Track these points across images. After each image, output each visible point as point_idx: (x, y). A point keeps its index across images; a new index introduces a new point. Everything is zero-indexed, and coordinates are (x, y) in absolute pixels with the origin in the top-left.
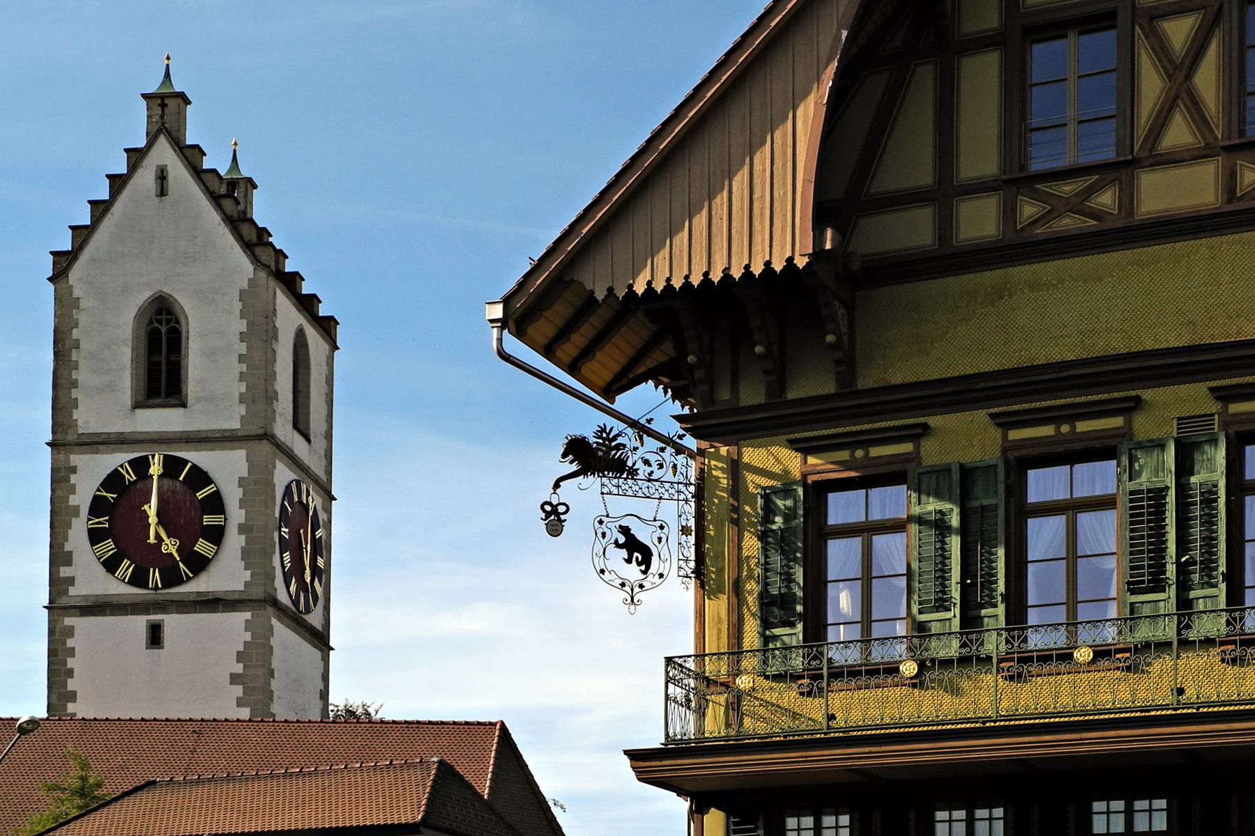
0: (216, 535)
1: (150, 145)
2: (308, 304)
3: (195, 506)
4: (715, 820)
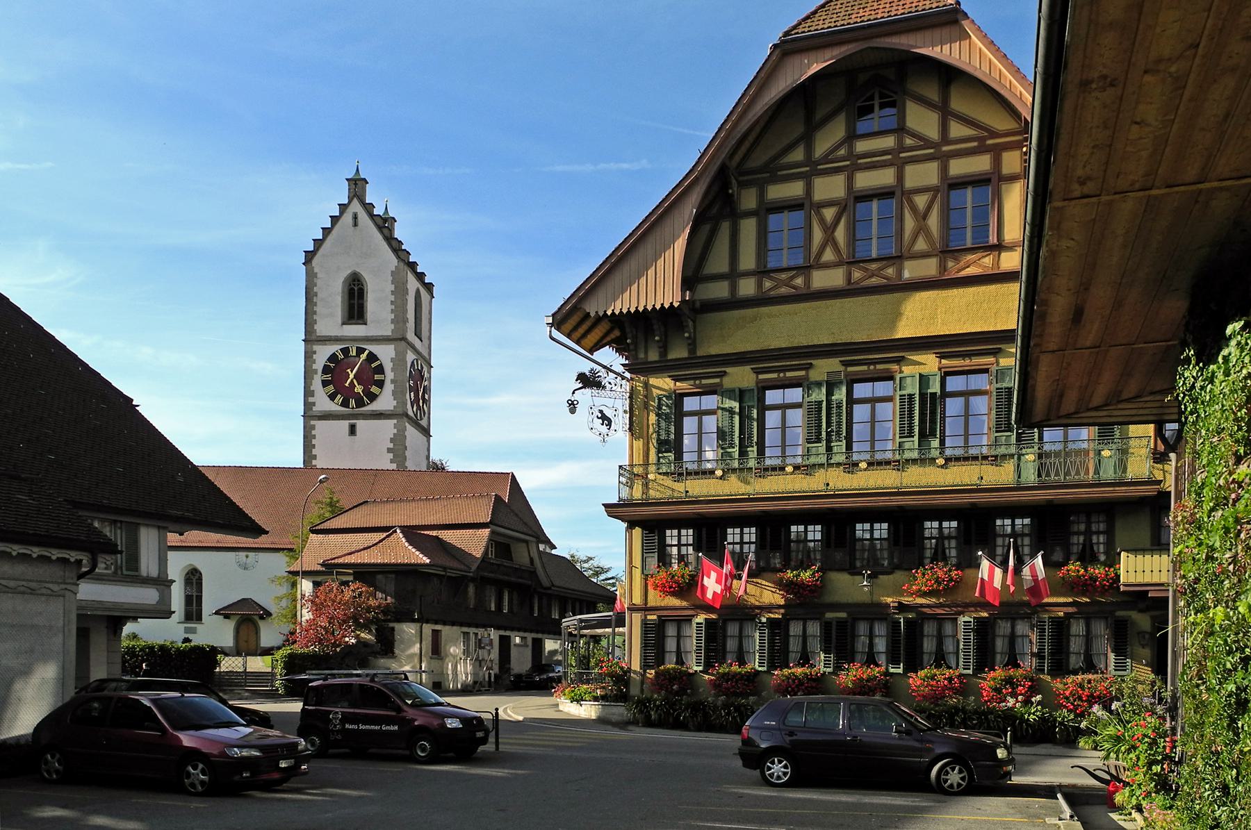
0: (380, 384)
1: (350, 202)
2: (420, 277)
3: (372, 373)
4: (637, 532)
